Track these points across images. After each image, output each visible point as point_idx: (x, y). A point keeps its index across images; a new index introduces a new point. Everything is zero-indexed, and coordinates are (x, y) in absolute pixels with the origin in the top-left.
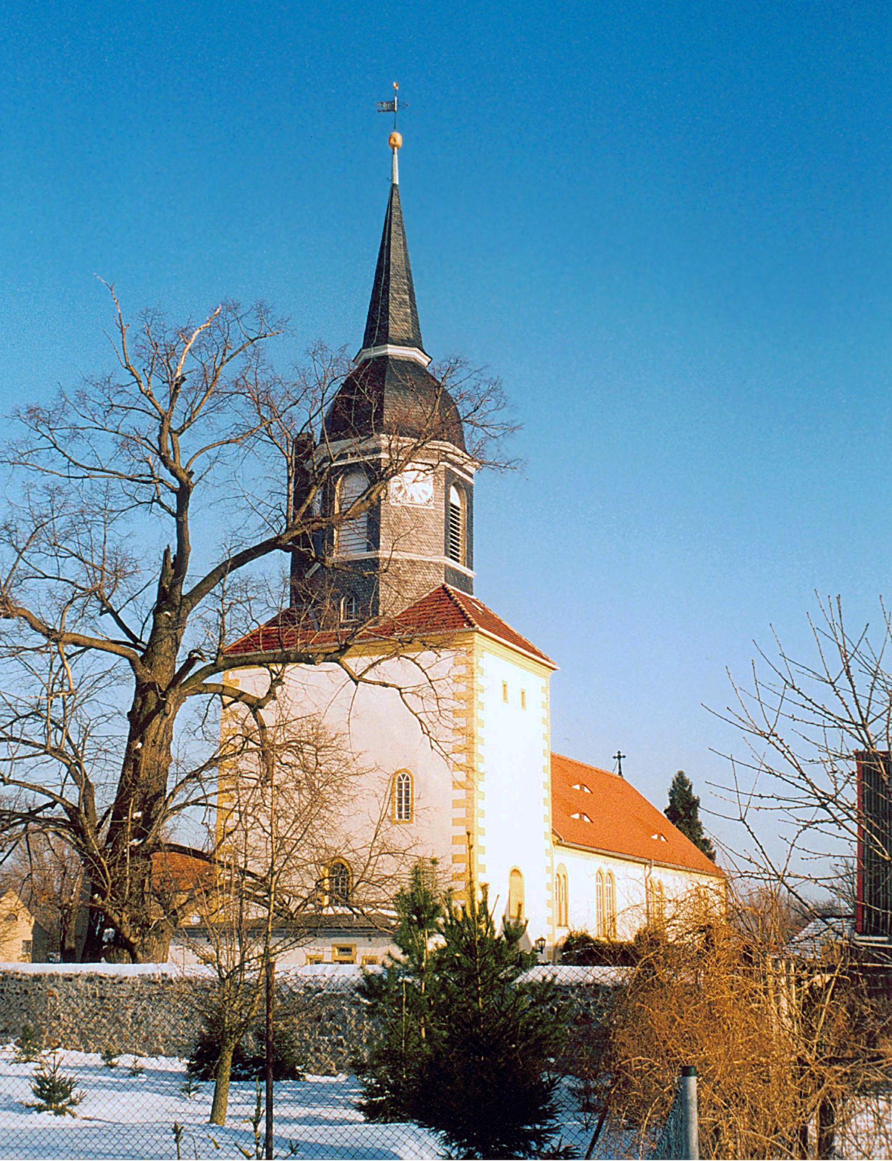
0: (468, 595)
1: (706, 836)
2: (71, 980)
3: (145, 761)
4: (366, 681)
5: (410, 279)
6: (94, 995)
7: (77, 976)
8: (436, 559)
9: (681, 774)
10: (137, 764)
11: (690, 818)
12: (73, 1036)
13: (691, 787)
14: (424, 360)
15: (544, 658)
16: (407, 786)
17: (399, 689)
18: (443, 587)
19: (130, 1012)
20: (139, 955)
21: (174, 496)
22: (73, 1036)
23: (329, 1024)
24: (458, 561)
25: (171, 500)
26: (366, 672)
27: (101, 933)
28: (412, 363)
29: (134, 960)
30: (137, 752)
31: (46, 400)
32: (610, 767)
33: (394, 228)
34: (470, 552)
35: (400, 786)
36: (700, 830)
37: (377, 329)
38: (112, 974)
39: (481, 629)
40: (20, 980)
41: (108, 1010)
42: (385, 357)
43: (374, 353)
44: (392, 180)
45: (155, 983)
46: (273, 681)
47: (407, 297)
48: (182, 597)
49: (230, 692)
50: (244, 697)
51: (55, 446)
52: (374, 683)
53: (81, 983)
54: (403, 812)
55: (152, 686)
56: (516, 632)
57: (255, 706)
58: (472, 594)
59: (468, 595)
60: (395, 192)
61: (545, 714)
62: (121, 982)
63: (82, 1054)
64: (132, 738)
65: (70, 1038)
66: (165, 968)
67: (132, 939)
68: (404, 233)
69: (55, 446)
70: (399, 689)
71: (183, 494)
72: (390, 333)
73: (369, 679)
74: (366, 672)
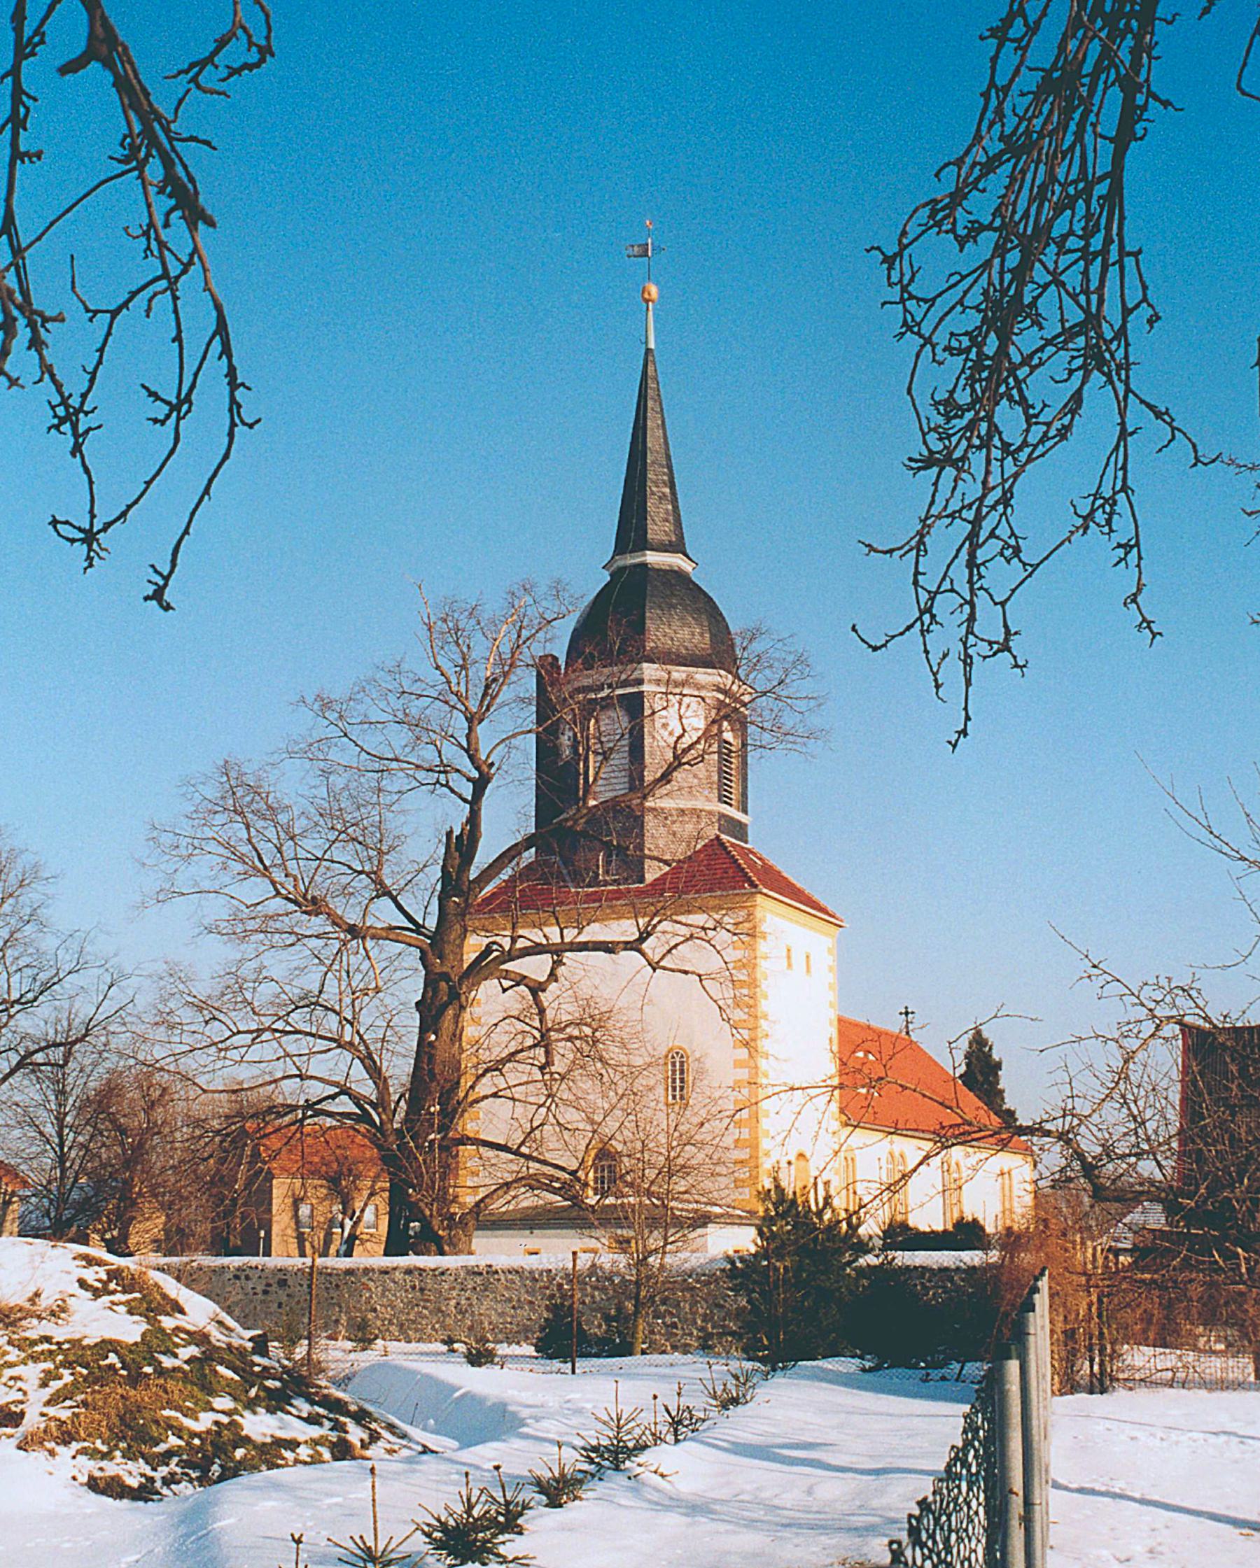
0: (742, 844)
1: (1009, 1104)
2: (386, 1273)
3: (441, 1054)
4: (664, 968)
5: (670, 467)
6: (414, 1287)
7: (395, 1269)
8: (709, 807)
9: (978, 1033)
10: (431, 1058)
11: (990, 1084)
12: (392, 1328)
13: (991, 1049)
14: (687, 566)
15: (830, 915)
16: (682, 1063)
17: (699, 976)
18: (718, 837)
19: (453, 1302)
20: (446, 1248)
21: (471, 785)
22: (392, 1328)
23: (663, 1308)
24: (731, 805)
25: (468, 790)
26: (662, 959)
27: (407, 1227)
28: (676, 572)
29: (442, 1253)
30: (431, 1044)
31: (337, 692)
32: (894, 1025)
33: (650, 404)
34: (744, 795)
35: (674, 1064)
36: (1003, 1099)
37: (632, 531)
38: (433, 1267)
39: (765, 891)
40: (330, 1275)
41: (428, 1301)
42: (644, 565)
43: (631, 560)
44: (646, 343)
45: (481, 1274)
46: (554, 962)
47: (667, 490)
48: (470, 882)
49: (513, 976)
50: (526, 981)
51: (346, 735)
52: (673, 970)
53: (398, 1276)
54: (677, 1093)
55: (446, 977)
56: (799, 885)
57: (536, 989)
58: (746, 842)
59: (742, 844)
60: (650, 358)
61: (831, 978)
62: (443, 1273)
63: (403, 1344)
64: (423, 1030)
65: (388, 1330)
66: (471, 1261)
67: (440, 1232)
68: (662, 409)
69: (346, 735)
70: (699, 976)
71: (480, 785)
72: (649, 536)
73: (669, 966)
74: (662, 959)
